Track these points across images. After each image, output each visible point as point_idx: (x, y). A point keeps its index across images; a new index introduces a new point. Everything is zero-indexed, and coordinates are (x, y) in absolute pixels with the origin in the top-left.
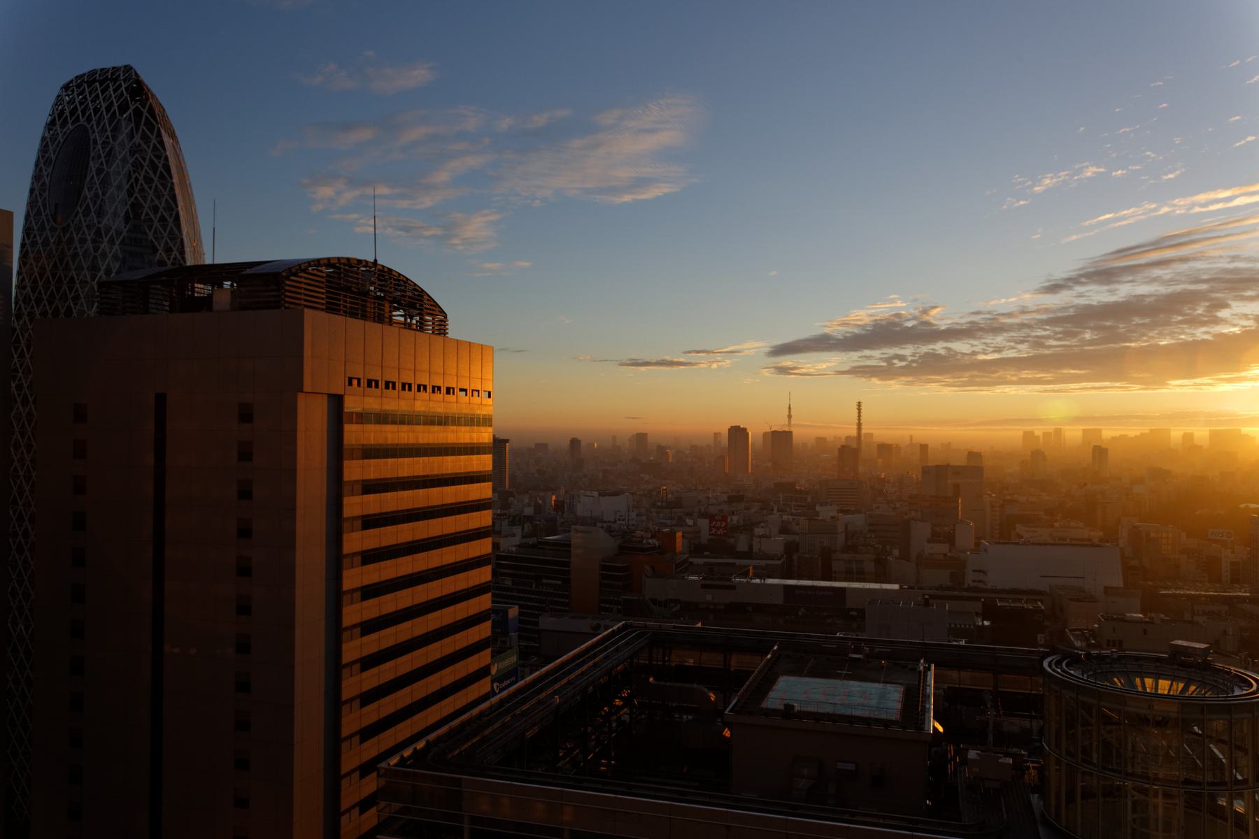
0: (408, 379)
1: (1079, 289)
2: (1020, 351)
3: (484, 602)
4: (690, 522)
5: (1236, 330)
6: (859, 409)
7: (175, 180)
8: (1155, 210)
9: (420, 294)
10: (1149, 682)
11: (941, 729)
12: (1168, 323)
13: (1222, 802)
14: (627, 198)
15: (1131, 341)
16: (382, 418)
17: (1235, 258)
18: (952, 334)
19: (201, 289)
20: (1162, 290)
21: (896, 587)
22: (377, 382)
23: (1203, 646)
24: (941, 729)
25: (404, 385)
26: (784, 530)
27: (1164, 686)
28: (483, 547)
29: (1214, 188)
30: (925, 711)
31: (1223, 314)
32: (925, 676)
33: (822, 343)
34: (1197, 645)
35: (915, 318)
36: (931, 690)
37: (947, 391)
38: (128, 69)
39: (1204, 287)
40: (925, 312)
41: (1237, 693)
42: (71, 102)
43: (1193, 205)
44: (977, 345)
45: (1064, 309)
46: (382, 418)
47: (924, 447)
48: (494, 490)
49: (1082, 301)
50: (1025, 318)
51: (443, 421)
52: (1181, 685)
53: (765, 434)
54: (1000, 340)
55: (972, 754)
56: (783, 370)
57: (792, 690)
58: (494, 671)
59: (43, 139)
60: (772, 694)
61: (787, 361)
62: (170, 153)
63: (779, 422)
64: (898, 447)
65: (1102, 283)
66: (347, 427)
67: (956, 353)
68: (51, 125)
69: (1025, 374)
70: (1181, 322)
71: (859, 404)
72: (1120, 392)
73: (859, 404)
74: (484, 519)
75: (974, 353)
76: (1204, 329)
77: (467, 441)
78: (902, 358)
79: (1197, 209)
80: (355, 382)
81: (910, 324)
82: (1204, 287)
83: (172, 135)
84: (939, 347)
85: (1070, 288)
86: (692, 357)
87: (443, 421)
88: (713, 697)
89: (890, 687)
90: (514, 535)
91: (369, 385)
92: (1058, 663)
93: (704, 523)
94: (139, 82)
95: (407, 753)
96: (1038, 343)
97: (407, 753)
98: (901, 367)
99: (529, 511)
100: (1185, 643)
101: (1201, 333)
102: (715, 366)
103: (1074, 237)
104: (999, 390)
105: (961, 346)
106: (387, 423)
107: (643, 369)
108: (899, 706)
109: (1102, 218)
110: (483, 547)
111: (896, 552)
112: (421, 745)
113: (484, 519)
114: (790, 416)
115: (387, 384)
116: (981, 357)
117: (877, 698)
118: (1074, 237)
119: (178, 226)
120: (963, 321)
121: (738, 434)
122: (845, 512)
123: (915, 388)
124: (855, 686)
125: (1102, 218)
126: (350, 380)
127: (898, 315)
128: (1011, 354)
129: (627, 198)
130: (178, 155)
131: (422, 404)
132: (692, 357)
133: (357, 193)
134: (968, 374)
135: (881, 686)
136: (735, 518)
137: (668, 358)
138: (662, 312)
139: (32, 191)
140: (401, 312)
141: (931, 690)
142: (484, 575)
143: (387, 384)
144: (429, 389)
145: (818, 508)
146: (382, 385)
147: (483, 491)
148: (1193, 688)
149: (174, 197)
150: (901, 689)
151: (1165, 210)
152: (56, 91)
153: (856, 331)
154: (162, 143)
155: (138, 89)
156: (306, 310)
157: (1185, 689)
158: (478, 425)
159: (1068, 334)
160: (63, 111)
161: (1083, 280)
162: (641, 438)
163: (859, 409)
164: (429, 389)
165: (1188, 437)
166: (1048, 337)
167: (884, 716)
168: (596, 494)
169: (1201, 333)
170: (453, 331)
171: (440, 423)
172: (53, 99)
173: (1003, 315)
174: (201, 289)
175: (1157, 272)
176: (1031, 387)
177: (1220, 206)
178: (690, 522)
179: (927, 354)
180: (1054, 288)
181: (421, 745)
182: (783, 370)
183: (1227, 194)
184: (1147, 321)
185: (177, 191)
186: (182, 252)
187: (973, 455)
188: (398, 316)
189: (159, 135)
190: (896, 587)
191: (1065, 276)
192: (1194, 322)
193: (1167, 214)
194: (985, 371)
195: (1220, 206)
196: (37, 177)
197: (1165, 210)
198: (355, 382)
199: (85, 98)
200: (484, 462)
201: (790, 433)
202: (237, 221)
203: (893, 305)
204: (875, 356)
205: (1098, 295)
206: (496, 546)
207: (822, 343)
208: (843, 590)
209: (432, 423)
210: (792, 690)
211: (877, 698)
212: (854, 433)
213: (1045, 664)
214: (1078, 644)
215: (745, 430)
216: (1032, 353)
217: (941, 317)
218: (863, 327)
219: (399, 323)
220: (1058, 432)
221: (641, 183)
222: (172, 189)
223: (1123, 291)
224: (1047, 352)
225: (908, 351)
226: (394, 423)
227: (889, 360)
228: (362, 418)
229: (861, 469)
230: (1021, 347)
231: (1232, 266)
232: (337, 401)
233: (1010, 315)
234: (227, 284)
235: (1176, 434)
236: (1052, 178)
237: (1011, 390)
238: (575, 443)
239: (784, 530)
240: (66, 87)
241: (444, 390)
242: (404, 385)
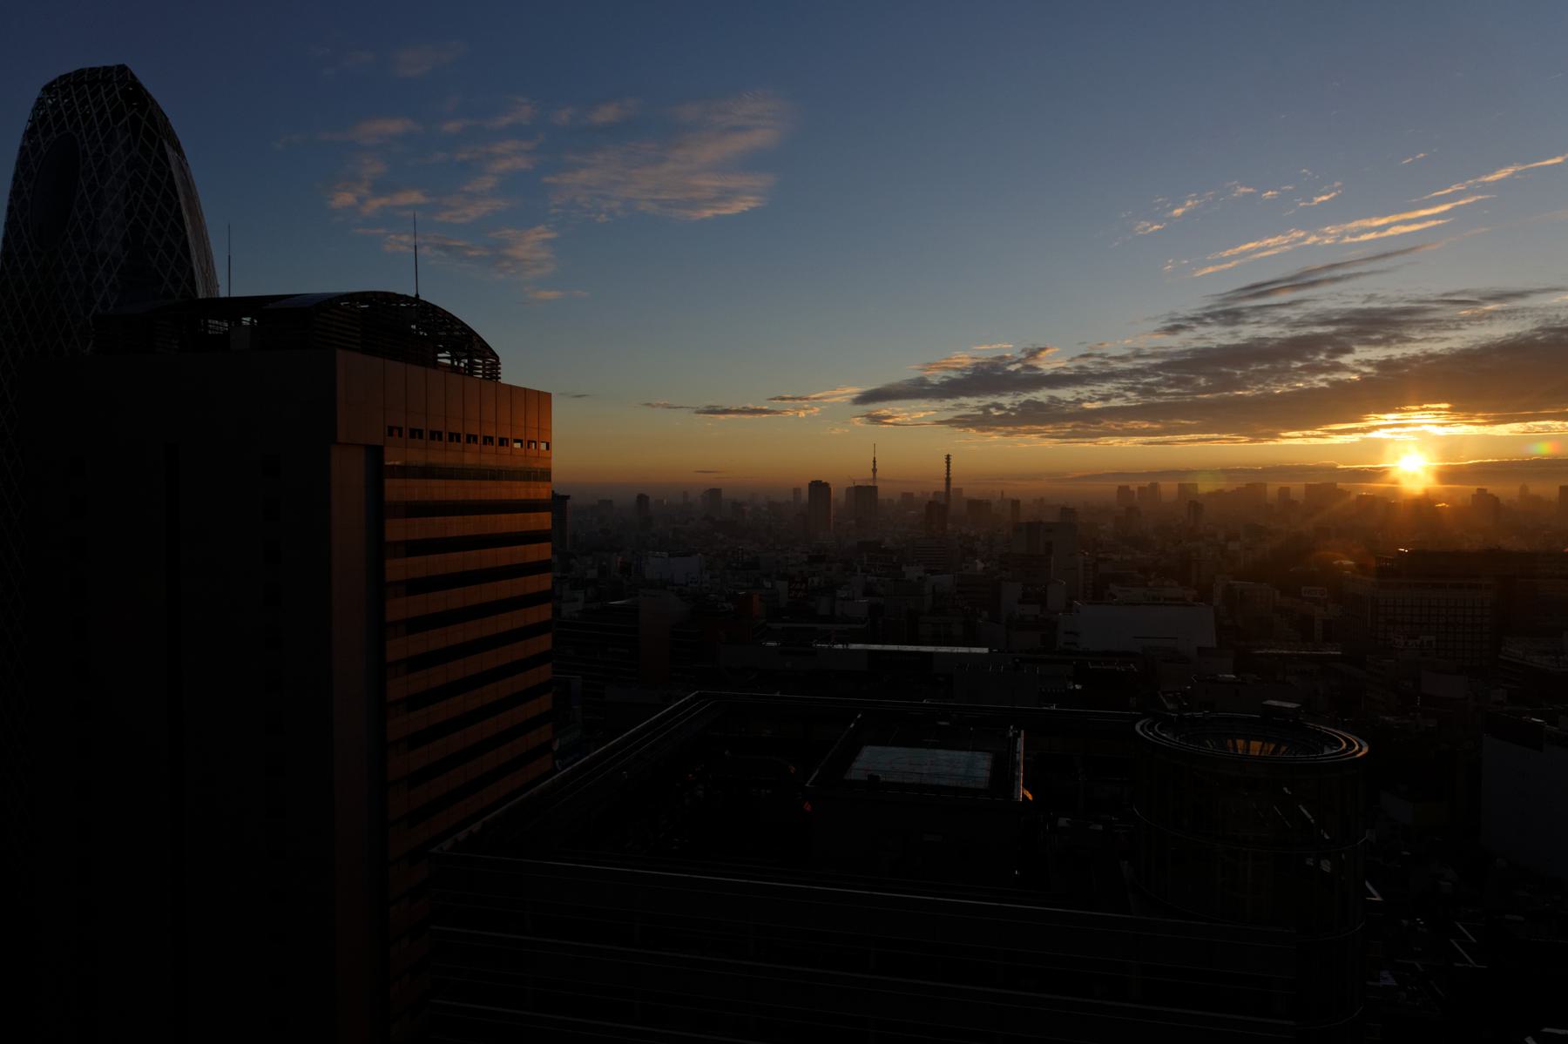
0: (474, 431)
1: (1201, 330)
2: (1128, 399)
3: (545, 672)
4: (768, 584)
5: (1355, 377)
6: (948, 463)
7: (182, 200)
8: (1304, 239)
9: (469, 334)
10: (1240, 743)
11: (1030, 797)
12: (1287, 370)
13: (1310, 862)
14: (708, 213)
15: (1245, 389)
16: (427, 472)
17: (1371, 298)
18: (1056, 380)
19: (218, 326)
20: (1288, 333)
21: (986, 650)
22: (400, 429)
23: (1294, 706)
24: (1030, 797)
25: (469, 437)
26: (869, 592)
27: (1256, 746)
28: (544, 613)
29: (1369, 216)
30: (1014, 778)
31: (1346, 359)
32: (1015, 743)
33: (917, 390)
34: (1289, 705)
35: (1019, 361)
36: (1020, 757)
37: (1049, 444)
38: (122, 69)
39: (1331, 329)
40: (1033, 354)
41: (1327, 752)
42: (55, 106)
43: (1343, 235)
44: (1085, 391)
45: (1183, 352)
46: (427, 472)
47: (1015, 503)
48: (554, 551)
49: (1200, 344)
50: (1139, 363)
51: (496, 475)
52: (1272, 746)
53: (848, 490)
54: (1107, 387)
55: (1063, 822)
56: (876, 419)
57: (879, 761)
58: (555, 748)
59: (22, 149)
60: (856, 765)
61: (883, 408)
62: (174, 169)
63: (862, 474)
64: (988, 504)
65: (1226, 324)
66: (387, 482)
67: (1060, 401)
68: (29, 134)
69: (1132, 424)
70: (1301, 368)
71: (948, 457)
72: (1227, 445)
73: (948, 457)
74: (544, 582)
75: (1079, 401)
76: (1322, 376)
77: (523, 497)
78: (999, 407)
79: (1348, 239)
80: (396, 432)
81: (1012, 368)
82: (1331, 329)
83: (177, 148)
84: (1042, 395)
85: (1191, 329)
86: (777, 405)
87: (496, 475)
88: (793, 770)
89: (978, 755)
90: (576, 600)
91: (432, 437)
92: (1151, 727)
93: (782, 586)
94: (138, 86)
95: (462, 836)
96: (1148, 391)
97: (462, 836)
98: (1000, 417)
99: (592, 574)
100: (1275, 703)
101: (1319, 381)
102: (802, 414)
103: (1210, 270)
104: (1104, 441)
105: (1066, 394)
106: (433, 477)
107: (722, 417)
108: (987, 774)
109: (1244, 247)
110: (544, 613)
111: (985, 614)
112: (476, 827)
113: (544, 582)
114: (874, 470)
115: (451, 435)
116: (1087, 405)
117: (966, 766)
118: (1210, 270)
119: (188, 255)
120: (1071, 365)
121: (819, 488)
122: (933, 572)
123: (1015, 438)
124: (942, 754)
125: (1244, 247)
126: (391, 429)
127: (1002, 358)
128: (1116, 402)
129: (708, 213)
130: (183, 168)
131: (471, 457)
132: (777, 405)
133: (384, 201)
134: (1070, 425)
135: (969, 754)
136: (816, 580)
137: (751, 406)
138: (754, 345)
139: (10, 209)
140: (447, 354)
141: (1020, 757)
142: (544, 643)
143: (451, 435)
144: (480, 440)
145: (904, 568)
146: (445, 436)
147: (543, 551)
148: (1284, 749)
149: (181, 220)
150: (989, 756)
151: (1313, 239)
152: (37, 92)
153: (953, 375)
154: (165, 156)
155: (136, 95)
156: (339, 351)
157: (1274, 751)
158: (536, 479)
159: (1179, 382)
160: (45, 115)
161: (1209, 320)
162: (714, 493)
163: (948, 463)
164: (480, 440)
165: (1284, 492)
166: (1158, 384)
167: (972, 786)
168: (665, 554)
169: (1319, 381)
170: (508, 376)
171: (493, 478)
172: (32, 104)
173: (1115, 358)
174: (218, 326)
175: (1286, 312)
176: (1136, 439)
177: (1372, 236)
178: (768, 584)
179: (1028, 402)
180: (1174, 330)
181: (476, 827)
182: (876, 419)
183: (1384, 221)
184: (1266, 366)
185: (184, 212)
186: (193, 284)
187: (1067, 511)
188: (444, 358)
189: (162, 147)
190: (986, 650)
191: (1189, 315)
192: (1315, 369)
193: (1315, 243)
194: (1086, 422)
195: (1372, 236)
196: (16, 193)
197: (1313, 239)
198: (396, 432)
199: (71, 101)
200: (544, 520)
201: (875, 488)
202: (258, 250)
203: (1002, 346)
204: (971, 404)
205: (1218, 336)
206: (557, 611)
207: (917, 390)
208: (931, 654)
209: (484, 478)
210: (879, 761)
211: (966, 766)
212: (943, 488)
213: (1138, 727)
214: (1170, 706)
215: (826, 485)
216: (1142, 401)
217: (1048, 364)
218: (965, 369)
219: (445, 365)
220: (1154, 487)
221: (726, 195)
222: (179, 211)
223: (1247, 332)
224: (1157, 400)
225: (1007, 400)
226: (440, 477)
227: (986, 409)
228: (405, 472)
229: (949, 526)
230: (1130, 394)
231: (1366, 306)
232: (376, 453)
233: (1122, 359)
234: (246, 320)
235: (1273, 488)
236: (1193, 199)
237: (1115, 441)
238: (642, 499)
239: (869, 592)
240: (48, 89)
241: (496, 441)
242: (469, 437)
